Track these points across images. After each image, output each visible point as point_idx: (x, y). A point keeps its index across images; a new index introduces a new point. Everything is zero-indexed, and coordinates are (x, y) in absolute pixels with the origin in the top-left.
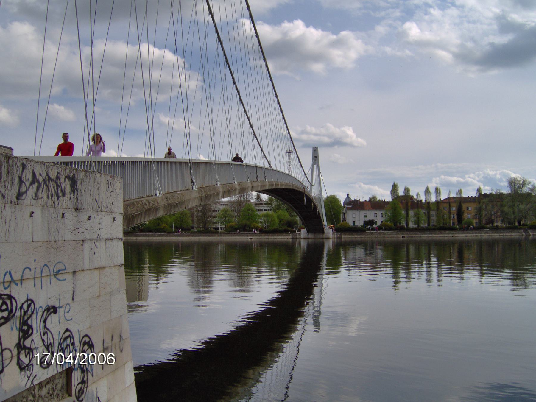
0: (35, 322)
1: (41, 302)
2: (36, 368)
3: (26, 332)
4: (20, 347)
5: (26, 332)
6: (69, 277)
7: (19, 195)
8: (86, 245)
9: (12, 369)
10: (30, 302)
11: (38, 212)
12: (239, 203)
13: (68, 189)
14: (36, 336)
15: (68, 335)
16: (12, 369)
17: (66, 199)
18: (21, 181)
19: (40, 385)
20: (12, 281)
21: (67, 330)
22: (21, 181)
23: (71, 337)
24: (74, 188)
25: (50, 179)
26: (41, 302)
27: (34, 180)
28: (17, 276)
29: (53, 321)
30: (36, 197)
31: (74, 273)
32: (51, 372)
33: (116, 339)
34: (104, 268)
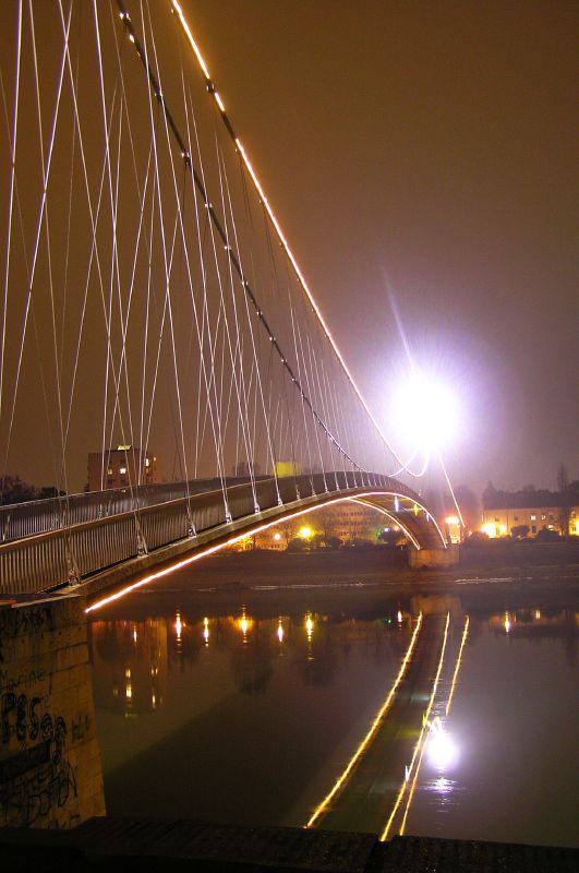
0: (27, 709)
1: (30, 695)
2: (28, 738)
3: (21, 716)
4: (19, 725)
5: (21, 716)
6: (47, 678)
7: (16, 632)
8: (59, 653)
9: (14, 738)
10: (23, 696)
11: (26, 639)
12: (153, 657)
13: (45, 618)
14: (27, 719)
15: (47, 717)
16: (14, 738)
17: (44, 625)
18: (17, 623)
19: (30, 750)
20: (14, 685)
21: (47, 714)
22: (17, 623)
23: (49, 718)
24: (49, 616)
25: (32, 614)
26: (30, 695)
27: (24, 619)
28: (16, 682)
29: (37, 707)
30: (25, 630)
31: (51, 674)
32: (37, 742)
33: (83, 720)
34: (73, 667)
